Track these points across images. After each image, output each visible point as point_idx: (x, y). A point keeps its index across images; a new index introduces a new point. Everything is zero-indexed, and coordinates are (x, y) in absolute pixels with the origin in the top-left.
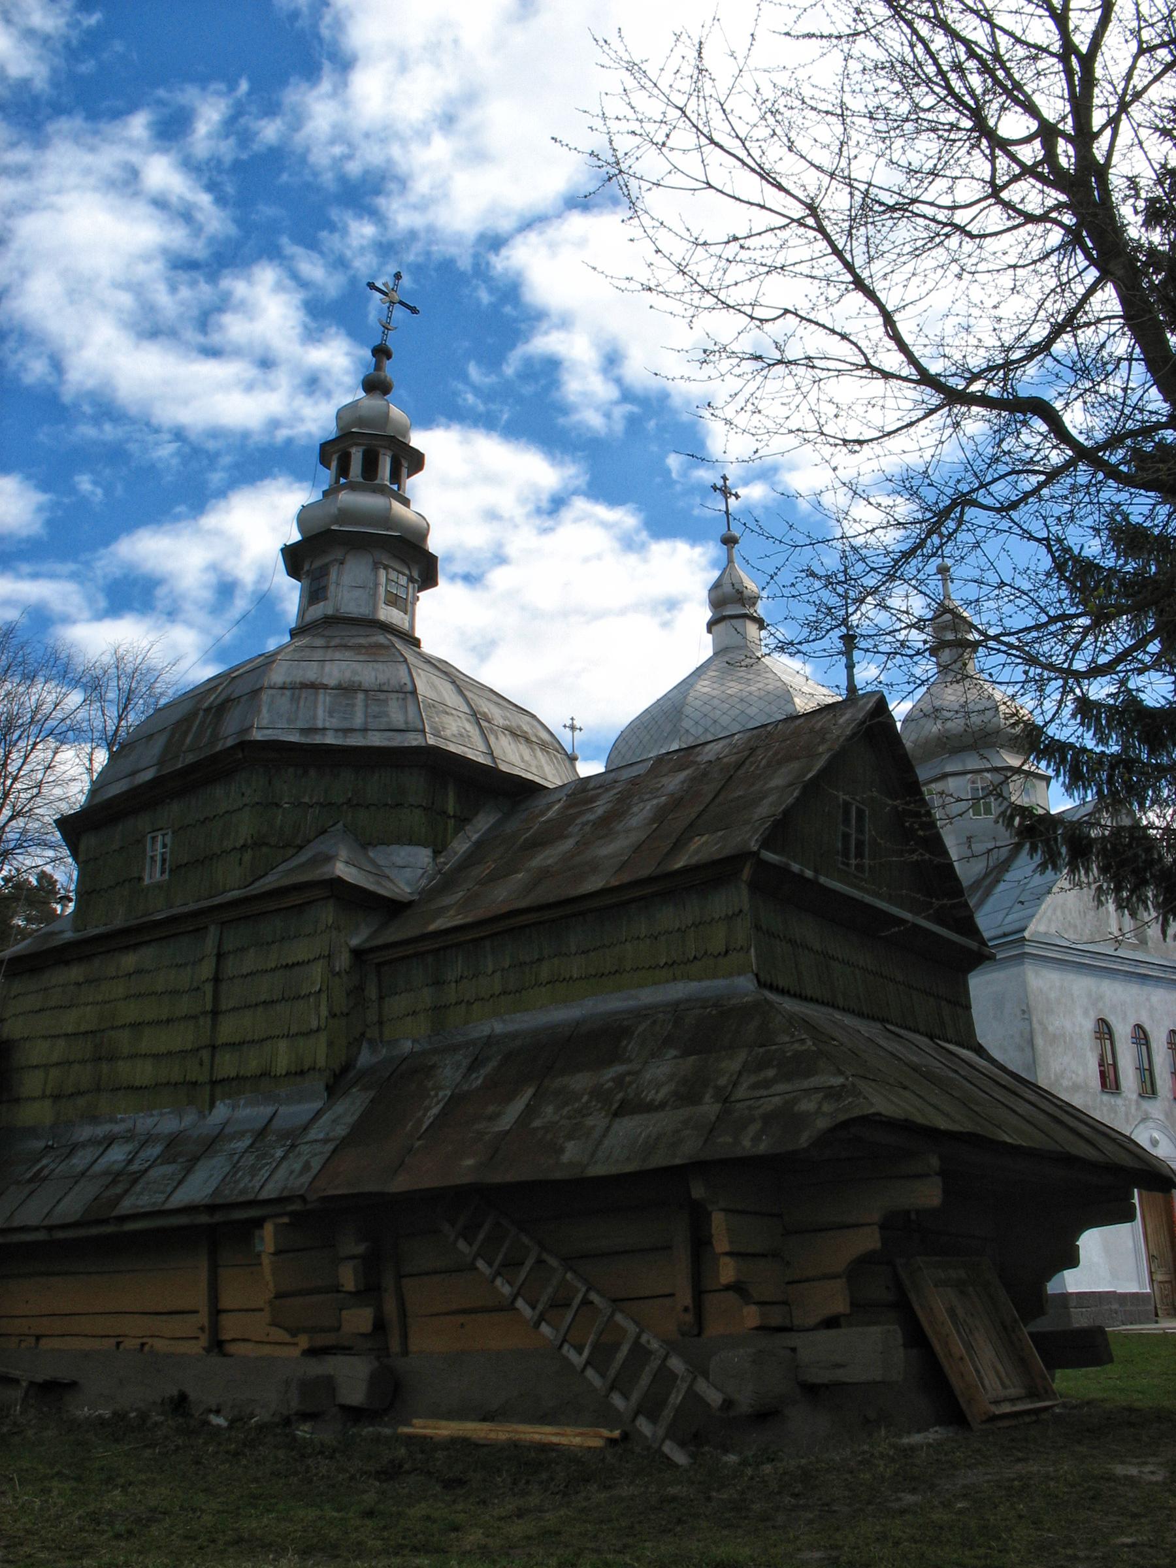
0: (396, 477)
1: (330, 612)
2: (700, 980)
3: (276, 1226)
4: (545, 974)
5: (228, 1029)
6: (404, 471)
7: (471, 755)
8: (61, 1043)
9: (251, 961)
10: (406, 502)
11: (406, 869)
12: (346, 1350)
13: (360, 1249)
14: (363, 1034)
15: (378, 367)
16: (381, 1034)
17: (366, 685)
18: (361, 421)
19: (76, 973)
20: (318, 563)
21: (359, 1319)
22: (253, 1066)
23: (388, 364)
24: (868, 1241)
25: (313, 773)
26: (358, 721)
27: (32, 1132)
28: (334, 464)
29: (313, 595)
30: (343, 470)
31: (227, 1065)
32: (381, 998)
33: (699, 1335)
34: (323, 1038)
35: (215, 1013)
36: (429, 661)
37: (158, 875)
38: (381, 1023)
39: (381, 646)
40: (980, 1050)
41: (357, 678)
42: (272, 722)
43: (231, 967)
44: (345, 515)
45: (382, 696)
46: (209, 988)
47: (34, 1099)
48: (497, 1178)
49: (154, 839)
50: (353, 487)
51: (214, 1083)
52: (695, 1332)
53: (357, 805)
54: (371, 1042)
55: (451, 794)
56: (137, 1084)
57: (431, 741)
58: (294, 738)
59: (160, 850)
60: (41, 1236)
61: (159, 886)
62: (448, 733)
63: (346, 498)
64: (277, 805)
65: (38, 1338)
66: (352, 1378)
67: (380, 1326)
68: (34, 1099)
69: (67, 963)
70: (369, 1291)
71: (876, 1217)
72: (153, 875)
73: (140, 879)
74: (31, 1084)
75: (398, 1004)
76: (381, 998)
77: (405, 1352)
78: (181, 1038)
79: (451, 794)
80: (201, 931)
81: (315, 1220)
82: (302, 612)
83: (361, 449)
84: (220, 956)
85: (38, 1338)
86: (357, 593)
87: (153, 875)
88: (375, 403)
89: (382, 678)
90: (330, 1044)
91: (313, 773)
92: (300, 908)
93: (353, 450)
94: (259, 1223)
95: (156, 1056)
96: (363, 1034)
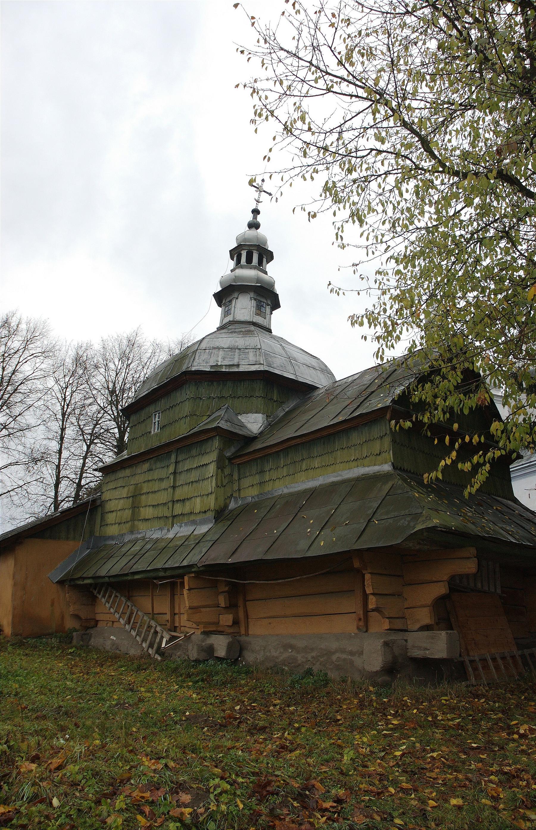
0: (260, 263)
1: (231, 319)
2: (368, 466)
3: (189, 577)
4: (304, 467)
5: (179, 494)
6: (265, 260)
7: (286, 375)
8: (122, 501)
9: (187, 465)
10: (266, 273)
11: (254, 422)
12: (221, 633)
13: (227, 589)
14: (232, 495)
15: (255, 218)
16: (239, 495)
17: (240, 347)
18: (245, 240)
19: (128, 472)
20: (228, 300)
21: (227, 619)
22: (187, 510)
23: (259, 217)
24: (441, 589)
25: (215, 383)
26: (235, 362)
27: (112, 538)
28: (235, 258)
29: (226, 314)
30: (238, 262)
31: (178, 509)
32: (239, 479)
33: (366, 631)
34: (213, 496)
35: (174, 487)
36: (275, 338)
37: (156, 430)
38: (239, 490)
39: (250, 331)
40: (516, 501)
41: (237, 344)
42: (202, 364)
43: (180, 468)
44: (237, 278)
45: (247, 351)
46: (172, 477)
47: (112, 524)
48: (269, 557)
49: (155, 415)
50: (242, 267)
51: (174, 517)
52: (365, 630)
53: (234, 397)
54: (236, 498)
55: (275, 391)
56: (147, 518)
57: (267, 369)
58: (208, 369)
59: (157, 419)
60: (107, 579)
61: (157, 434)
62: (275, 365)
63: (240, 272)
64: (201, 399)
65: (113, 622)
66: (221, 645)
67: (236, 622)
68: (112, 524)
69: (124, 468)
70: (232, 606)
71: (446, 578)
72: (155, 430)
73: (150, 432)
74: (111, 518)
75: (246, 482)
76: (239, 479)
77: (247, 634)
78: (163, 497)
79: (275, 391)
80: (169, 454)
81: (211, 574)
82: (222, 321)
83: (245, 251)
84: (176, 462)
85: (113, 622)
86: (243, 311)
87: (155, 430)
88: (253, 232)
89: (247, 343)
90: (216, 499)
91: (215, 383)
92: (207, 440)
93: (242, 252)
94: (182, 576)
95: (153, 506)
96: (232, 495)
